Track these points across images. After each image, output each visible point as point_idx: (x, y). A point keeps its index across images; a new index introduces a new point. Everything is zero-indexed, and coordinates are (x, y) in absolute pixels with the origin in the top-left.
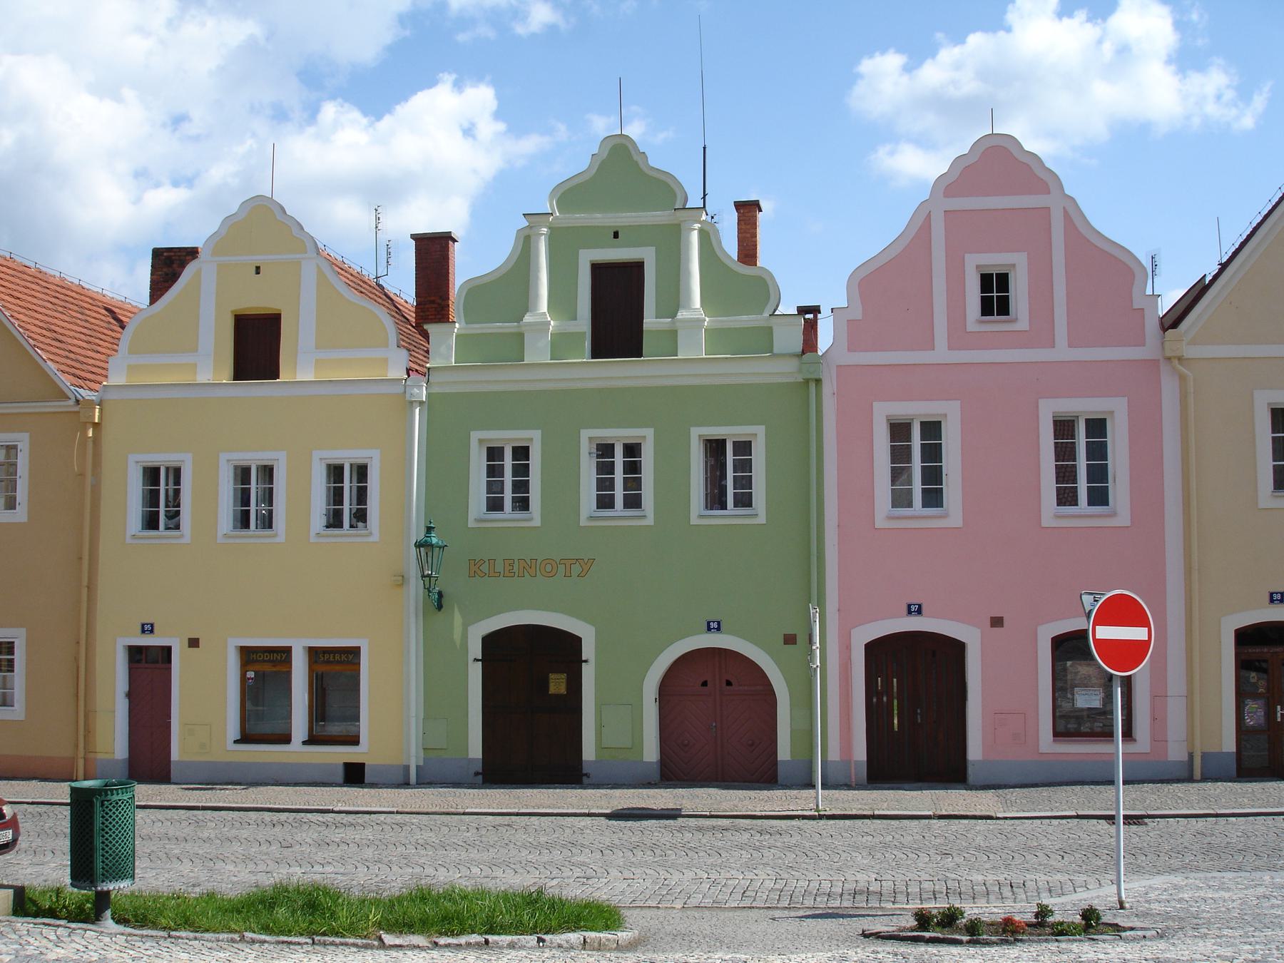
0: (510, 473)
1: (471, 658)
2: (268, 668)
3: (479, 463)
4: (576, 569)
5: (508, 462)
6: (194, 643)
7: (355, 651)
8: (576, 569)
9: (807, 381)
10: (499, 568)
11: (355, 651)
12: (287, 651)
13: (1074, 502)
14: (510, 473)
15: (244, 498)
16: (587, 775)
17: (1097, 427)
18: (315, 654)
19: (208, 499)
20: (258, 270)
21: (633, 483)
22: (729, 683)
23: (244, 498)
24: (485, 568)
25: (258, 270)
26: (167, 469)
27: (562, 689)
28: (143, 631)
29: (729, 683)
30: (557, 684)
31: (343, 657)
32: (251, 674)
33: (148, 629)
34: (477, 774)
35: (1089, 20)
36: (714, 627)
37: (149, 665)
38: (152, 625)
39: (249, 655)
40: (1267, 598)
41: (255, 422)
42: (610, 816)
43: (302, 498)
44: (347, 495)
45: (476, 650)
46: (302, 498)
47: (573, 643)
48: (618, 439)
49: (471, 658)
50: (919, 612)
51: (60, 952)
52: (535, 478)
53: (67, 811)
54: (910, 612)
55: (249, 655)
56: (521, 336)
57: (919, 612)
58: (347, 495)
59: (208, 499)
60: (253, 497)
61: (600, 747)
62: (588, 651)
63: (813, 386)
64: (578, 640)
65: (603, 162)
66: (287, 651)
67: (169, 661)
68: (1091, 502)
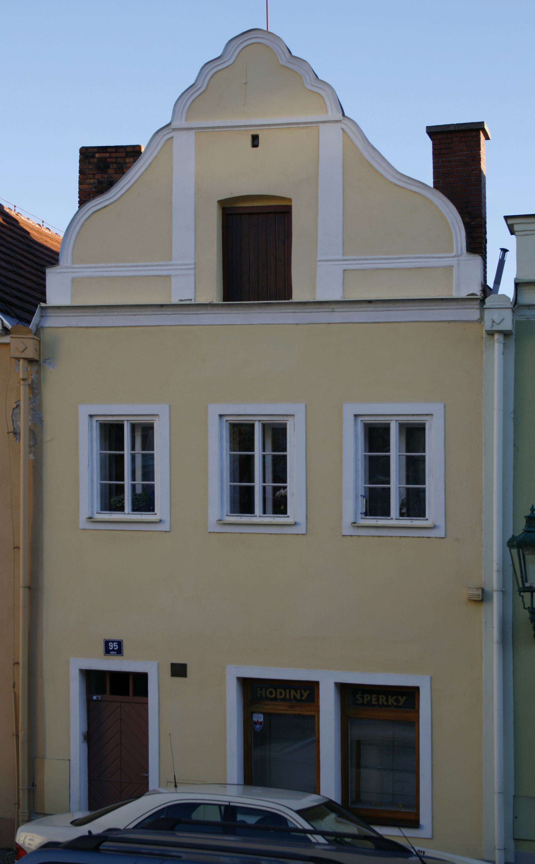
2: (280, 708)
6: (179, 670)
7: (411, 695)
11: (411, 695)
12: (311, 688)
17: (414, 434)
18: (351, 695)
19: (191, 469)
20: (255, 141)
23: (243, 469)
25: (255, 141)
26: (133, 426)
28: (107, 651)
31: (391, 700)
32: (259, 718)
33: (113, 648)
37: (115, 695)
38: (120, 643)
39: (253, 690)
40: (101, 648)
41: (256, 362)
43: (325, 470)
44: (393, 467)
46: (325, 470)
50: (119, 652)
55: (253, 690)
57: (119, 652)
58: (393, 467)
59: (191, 469)
66: (311, 688)
67: (145, 693)
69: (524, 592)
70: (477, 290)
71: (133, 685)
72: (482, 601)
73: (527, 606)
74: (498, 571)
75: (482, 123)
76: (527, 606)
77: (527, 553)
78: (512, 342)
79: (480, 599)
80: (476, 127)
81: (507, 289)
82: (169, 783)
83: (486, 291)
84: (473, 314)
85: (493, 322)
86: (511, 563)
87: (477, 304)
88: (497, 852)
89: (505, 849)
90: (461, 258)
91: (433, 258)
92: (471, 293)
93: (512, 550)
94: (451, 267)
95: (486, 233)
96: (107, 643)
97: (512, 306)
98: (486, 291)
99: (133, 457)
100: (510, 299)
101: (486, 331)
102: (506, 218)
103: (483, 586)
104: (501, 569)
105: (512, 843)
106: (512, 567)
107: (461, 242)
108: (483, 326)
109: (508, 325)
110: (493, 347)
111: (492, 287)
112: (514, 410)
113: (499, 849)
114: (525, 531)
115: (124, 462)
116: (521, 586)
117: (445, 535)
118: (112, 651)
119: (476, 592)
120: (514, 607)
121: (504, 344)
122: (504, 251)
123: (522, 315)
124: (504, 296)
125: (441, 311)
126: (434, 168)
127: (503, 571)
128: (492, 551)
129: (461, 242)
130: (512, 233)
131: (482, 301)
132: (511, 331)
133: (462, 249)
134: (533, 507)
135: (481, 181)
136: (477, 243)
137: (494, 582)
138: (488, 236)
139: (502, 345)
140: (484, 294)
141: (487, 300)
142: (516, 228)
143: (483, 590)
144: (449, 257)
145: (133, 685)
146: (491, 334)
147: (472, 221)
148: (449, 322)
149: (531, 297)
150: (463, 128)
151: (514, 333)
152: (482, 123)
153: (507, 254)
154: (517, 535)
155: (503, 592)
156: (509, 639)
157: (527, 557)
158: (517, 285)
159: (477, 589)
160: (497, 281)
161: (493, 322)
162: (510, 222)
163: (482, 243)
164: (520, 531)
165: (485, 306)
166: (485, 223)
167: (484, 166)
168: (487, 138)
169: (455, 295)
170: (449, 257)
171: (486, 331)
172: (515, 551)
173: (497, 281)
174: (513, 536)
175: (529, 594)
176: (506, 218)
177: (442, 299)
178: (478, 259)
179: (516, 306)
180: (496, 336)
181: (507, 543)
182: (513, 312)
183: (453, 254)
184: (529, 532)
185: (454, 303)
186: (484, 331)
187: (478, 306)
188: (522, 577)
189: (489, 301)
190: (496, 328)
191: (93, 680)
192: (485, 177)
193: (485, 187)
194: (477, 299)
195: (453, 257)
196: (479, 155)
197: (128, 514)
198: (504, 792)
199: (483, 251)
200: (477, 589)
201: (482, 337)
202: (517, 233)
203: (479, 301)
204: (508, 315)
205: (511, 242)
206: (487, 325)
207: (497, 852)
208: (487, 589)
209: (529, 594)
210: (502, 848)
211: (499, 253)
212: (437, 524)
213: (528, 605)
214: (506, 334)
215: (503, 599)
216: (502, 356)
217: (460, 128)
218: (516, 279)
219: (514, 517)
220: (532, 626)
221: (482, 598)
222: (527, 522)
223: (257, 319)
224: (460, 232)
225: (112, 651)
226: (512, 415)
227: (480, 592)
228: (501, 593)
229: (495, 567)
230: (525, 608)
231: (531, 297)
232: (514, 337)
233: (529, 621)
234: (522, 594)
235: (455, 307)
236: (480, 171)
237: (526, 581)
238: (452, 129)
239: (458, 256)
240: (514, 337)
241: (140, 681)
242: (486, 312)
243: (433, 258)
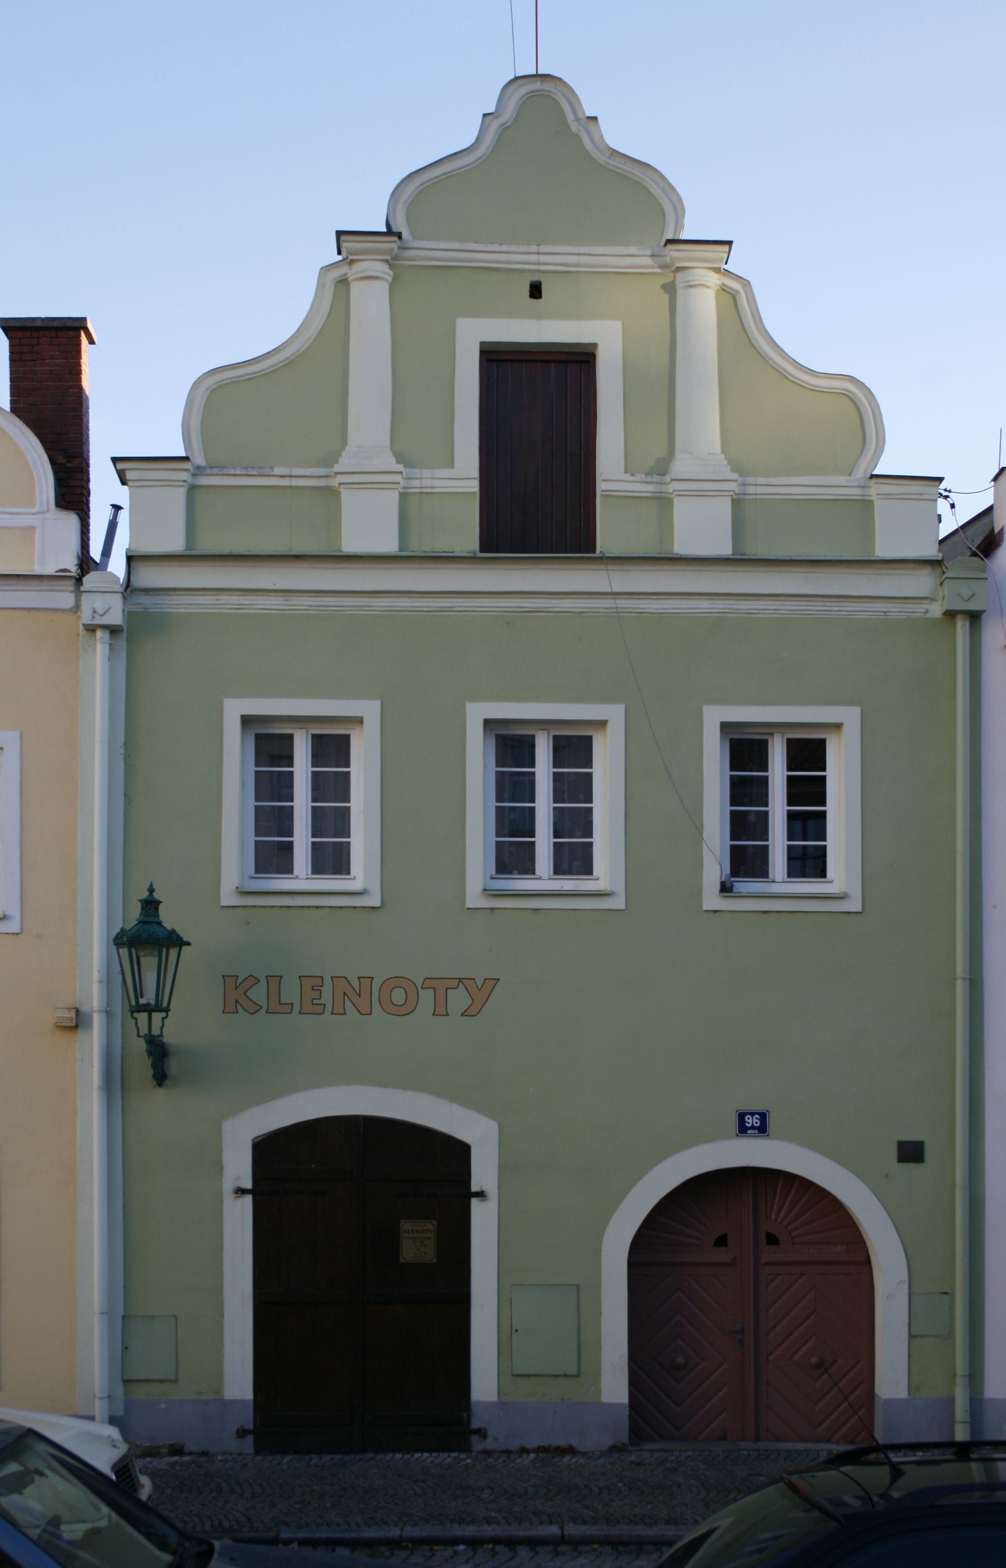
0: (294, 773)
1: (228, 1186)
3: (236, 764)
4: (459, 1000)
8: (459, 1000)
9: (951, 615)
10: (290, 993)
13: (528, 867)
14: (294, 773)
16: (482, 1433)
21: (808, 822)
22: (772, 1240)
24: (259, 994)
27: (429, 1254)
29: (772, 1240)
30: (417, 1242)
34: (242, 1433)
36: (753, 1124)
38: (763, 1116)
45: (239, 1167)
47: (456, 1154)
48: (544, 724)
49: (228, 1186)
50: (762, 1129)
51: (551, 1564)
54: (743, 1129)
56: (331, 495)
60: (538, 781)
61: (509, 1373)
62: (483, 1173)
63: (962, 627)
64: (461, 1151)
65: (504, 130)
68: (560, 869)
69: (138, 1011)
70: (71, 564)
72: (76, 1027)
73: (142, 1033)
74: (100, 982)
75: (84, 319)
76: (142, 1033)
77: (143, 953)
78: (122, 642)
79: (74, 1024)
80: (75, 324)
81: (117, 566)
83: (86, 564)
84: (65, 598)
85: (94, 612)
86: (119, 969)
87: (70, 585)
88: (97, 1402)
89: (109, 1397)
90: (47, 516)
91: (6, 513)
92: (62, 567)
93: (121, 951)
94: (32, 528)
95: (88, 480)
96: (741, 1116)
97: (122, 590)
98: (86, 564)
100: (118, 578)
101: (83, 625)
102: (115, 460)
103: (78, 1005)
104: (105, 979)
105: (120, 1387)
106: (121, 976)
107: (47, 493)
108: (79, 617)
109: (116, 618)
110: (95, 650)
111: (98, 561)
112: (125, 744)
113: (100, 1398)
114: (140, 922)
116: (133, 1003)
117: (22, 929)
118: (749, 1128)
119: (67, 1015)
120: (124, 1035)
121: (111, 645)
122: (117, 508)
123: (141, 604)
124: (111, 574)
125: (16, 593)
126: (12, 380)
127: (108, 982)
128: (92, 952)
129: (47, 493)
130: (124, 482)
131: (79, 581)
132: (120, 626)
133: (48, 502)
134: (151, 886)
135: (81, 404)
136: (72, 492)
137: (94, 999)
138: (92, 486)
139: (107, 646)
140: (82, 571)
141: (85, 579)
142: (129, 475)
143: (78, 1011)
144: (29, 514)
146: (91, 629)
147: (69, 462)
148: (29, 610)
149: (149, 577)
150: (56, 324)
151: (125, 629)
152: (84, 319)
153: (121, 513)
154: (128, 928)
155: (108, 1013)
156: (116, 1082)
157: (142, 959)
158: (130, 559)
159: (69, 1009)
160: (106, 552)
161: (94, 612)
162: (121, 466)
163: (83, 495)
164: (132, 922)
165: (82, 589)
166: (88, 466)
167: (86, 383)
168: (91, 341)
169: (38, 570)
170: (29, 514)
171: (83, 625)
172: (124, 952)
173: (106, 552)
174: (122, 929)
175: (146, 1014)
176: (115, 460)
177: (18, 576)
178: (72, 520)
179: (129, 590)
180: (99, 633)
181: (114, 940)
182: (124, 598)
183: (35, 510)
184: (145, 923)
185: (35, 582)
186: (81, 627)
187: (72, 588)
188: (135, 990)
189: (90, 580)
190: (98, 621)
192: (87, 399)
193: (87, 412)
194: (71, 577)
195: (35, 514)
196: (79, 365)
198: (107, 1313)
199: (85, 509)
200: (69, 1009)
201: (78, 634)
202: (130, 483)
203: (74, 581)
204: (116, 603)
205: (122, 495)
206: (86, 617)
207: (97, 1402)
208: (84, 1009)
209: (146, 1014)
210: (106, 1395)
211: (109, 512)
212: (8, 913)
213: (144, 1031)
214: (114, 631)
215: (108, 1024)
216: (107, 663)
217: (51, 324)
218: (128, 550)
219: (124, 901)
220: (150, 1061)
221: (77, 1022)
222: (142, 909)
224: (46, 478)
225: (749, 1128)
226: (122, 751)
227: (73, 1014)
228: (104, 1015)
229: (96, 976)
230: (139, 1036)
231: (149, 577)
232: (125, 635)
233: (146, 1054)
234: (135, 1015)
235: (37, 588)
236: (81, 389)
237: (142, 996)
238: (38, 324)
239: (43, 513)
240: (125, 635)
242: (84, 597)
243: (6, 513)
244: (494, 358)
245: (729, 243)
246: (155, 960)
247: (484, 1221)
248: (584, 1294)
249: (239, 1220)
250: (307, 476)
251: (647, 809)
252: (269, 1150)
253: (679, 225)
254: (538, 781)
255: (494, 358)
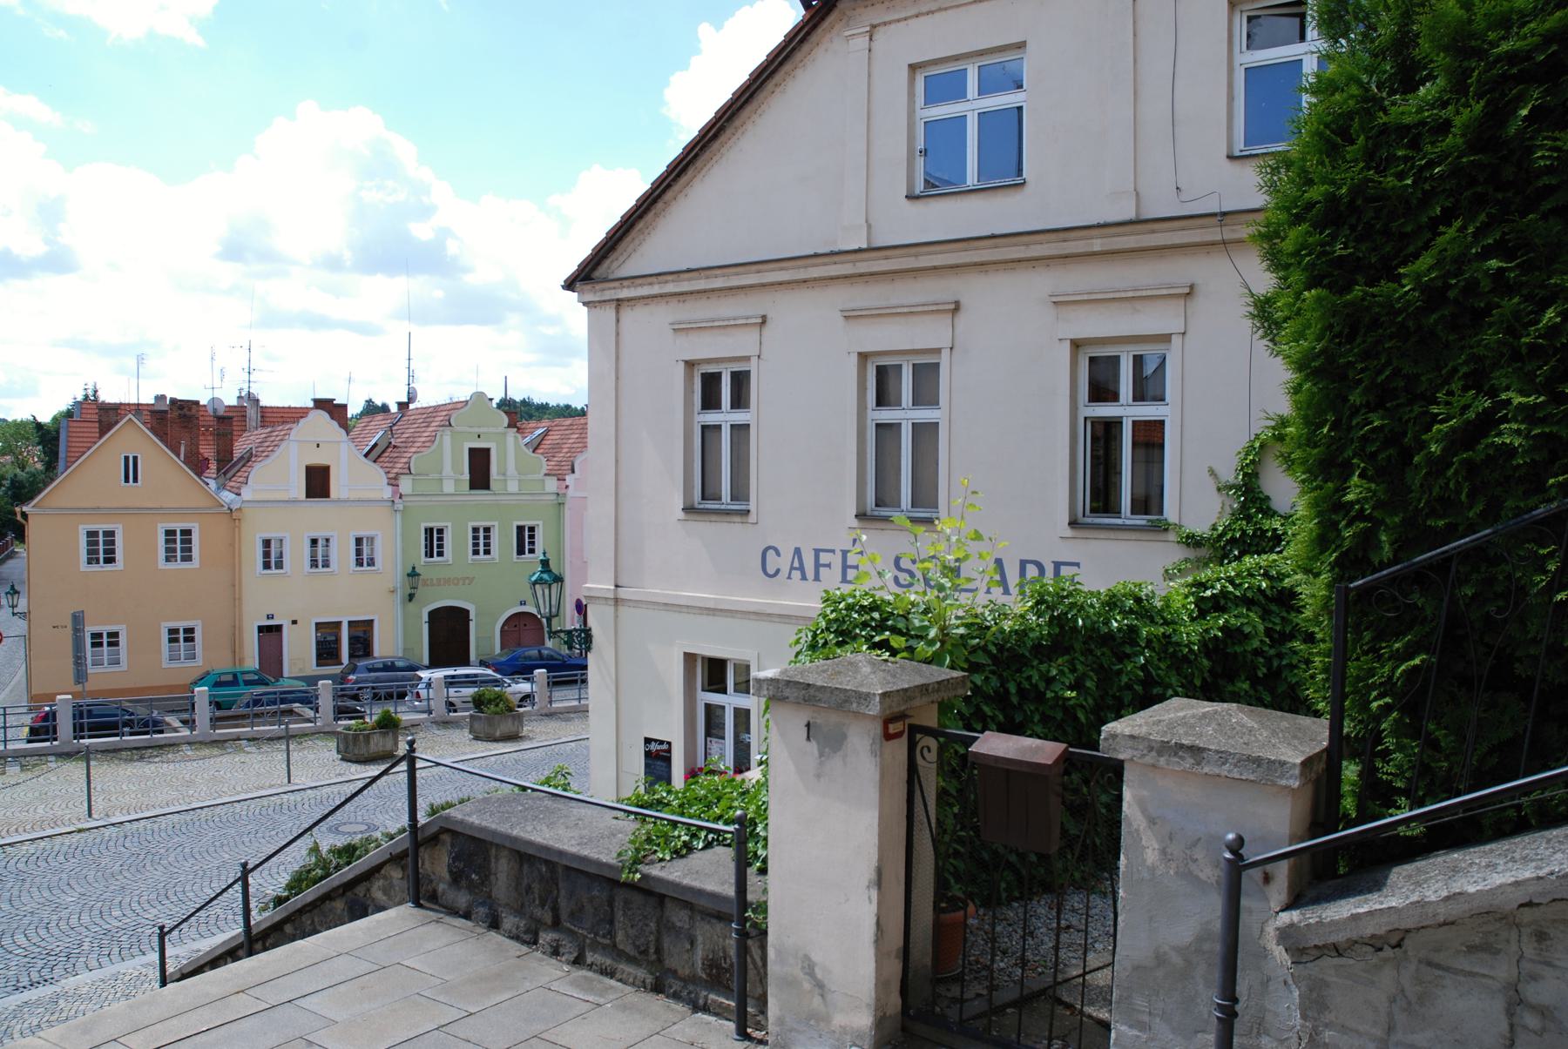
0: (434, 541)
5: (481, 534)
6: (294, 622)
14: (434, 541)
15: (487, 538)
19: (296, 555)
33: (270, 617)
35: (719, 27)
36: (523, 603)
41: (319, 518)
42: (254, 942)
43: (342, 553)
44: (362, 554)
45: (425, 618)
46: (342, 553)
52: (470, 542)
53: (103, 772)
58: (362, 554)
59: (296, 555)
60: (481, 540)
62: (472, 616)
64: (467, 612)
71: (278, 629)
82: (709, 492)
99: (90, 737)
115: (271, 557)
145: (278, 629)
159: (1297, 220)
191: (261, 629)
197: (274, 571)
207: (782, 764)
223: (318, 504)
241: (279, 628)
244: (471, 450)
245: (359, 541)
246: (282, 756)
247: (472, 624)
248: (492, 637)
249: (426, 628)
250: (436, 476)
251: (504, 541)
252: (432, 614)
253: (725, 899)
254: (481, 540)
255: (471, 450)
